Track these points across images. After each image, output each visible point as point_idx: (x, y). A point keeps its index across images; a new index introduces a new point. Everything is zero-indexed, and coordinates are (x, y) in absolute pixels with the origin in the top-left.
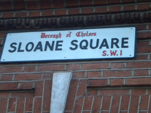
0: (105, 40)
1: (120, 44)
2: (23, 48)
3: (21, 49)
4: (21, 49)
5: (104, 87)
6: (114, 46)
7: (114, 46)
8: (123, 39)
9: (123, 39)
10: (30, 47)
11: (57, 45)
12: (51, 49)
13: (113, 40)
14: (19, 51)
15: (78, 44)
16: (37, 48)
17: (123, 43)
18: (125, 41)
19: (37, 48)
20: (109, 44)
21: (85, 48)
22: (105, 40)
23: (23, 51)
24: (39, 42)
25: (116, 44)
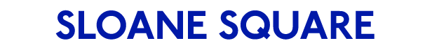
0: (314, 16)
1: (351, 28)
2: (90, 28)
3: (86, 32)
4: (86, 32)
5: (269, 26)
6: (338, 31)
7: (338, 31)
8: (359, 14)
9: (359, 14)
10: (111, 25)
11: (192, 24)
12: (178, 34)
13: (334, 14)
14: (82, 35)
15: (237, 21)
16: (135, 30)
17: (360, 24)
18: (364, 19)
19: (135, 30)
20: (327, 27)
21: (263, 33)
22: (314, 16)
23: (92, 36)
24: (162, 12)
25: (342, 26)
